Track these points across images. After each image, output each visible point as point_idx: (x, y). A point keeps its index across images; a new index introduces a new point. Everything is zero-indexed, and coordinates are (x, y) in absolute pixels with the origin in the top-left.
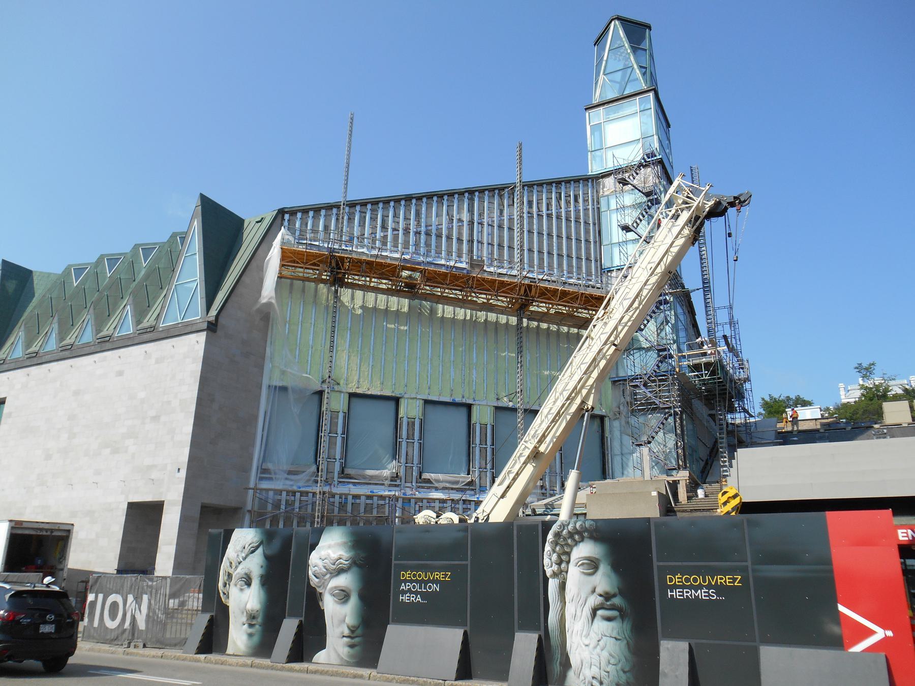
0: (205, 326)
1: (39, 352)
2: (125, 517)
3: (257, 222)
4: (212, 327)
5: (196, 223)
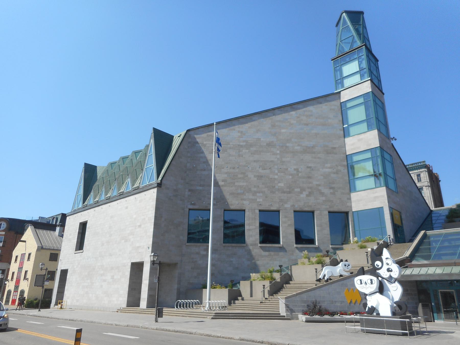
0: (156, 185)
1: (111, 196)
2: (130, 269)
3: (179, 137)
4: (159, 185)
5: (152, 140)
